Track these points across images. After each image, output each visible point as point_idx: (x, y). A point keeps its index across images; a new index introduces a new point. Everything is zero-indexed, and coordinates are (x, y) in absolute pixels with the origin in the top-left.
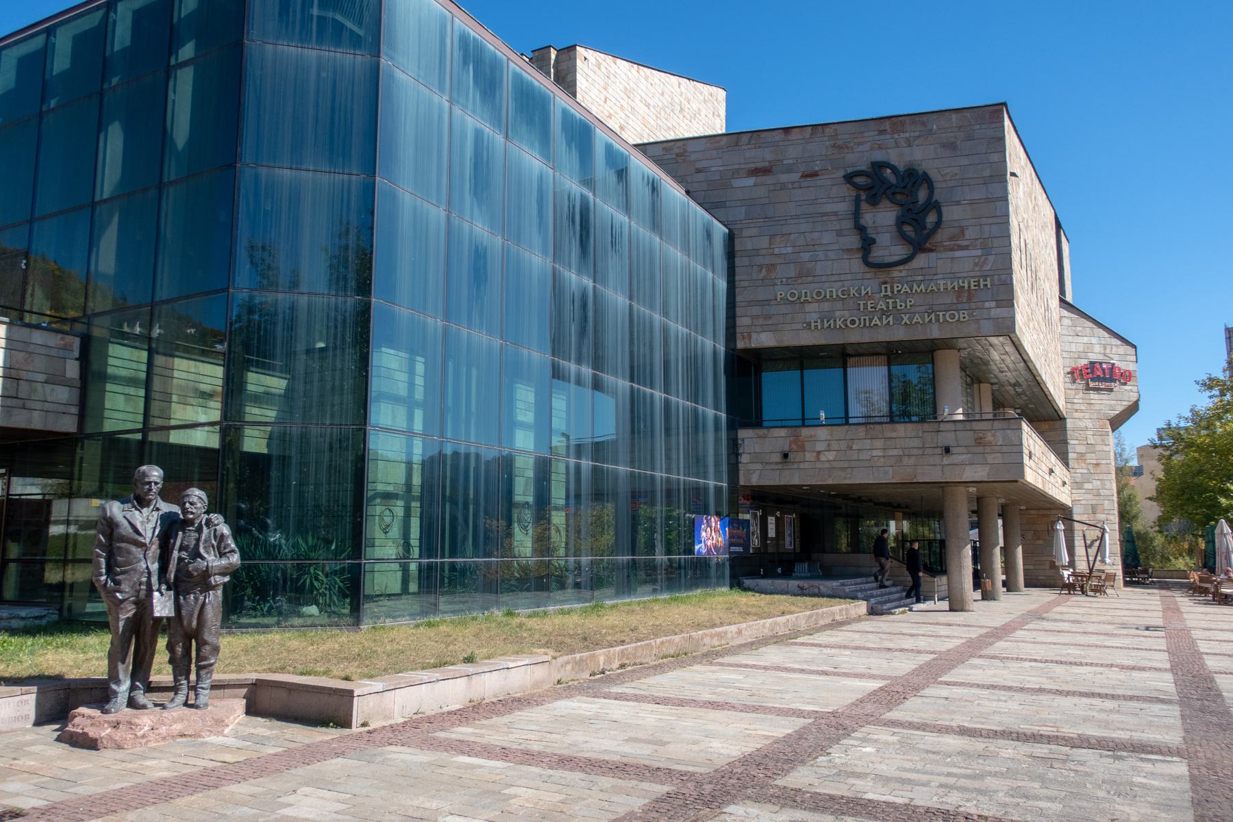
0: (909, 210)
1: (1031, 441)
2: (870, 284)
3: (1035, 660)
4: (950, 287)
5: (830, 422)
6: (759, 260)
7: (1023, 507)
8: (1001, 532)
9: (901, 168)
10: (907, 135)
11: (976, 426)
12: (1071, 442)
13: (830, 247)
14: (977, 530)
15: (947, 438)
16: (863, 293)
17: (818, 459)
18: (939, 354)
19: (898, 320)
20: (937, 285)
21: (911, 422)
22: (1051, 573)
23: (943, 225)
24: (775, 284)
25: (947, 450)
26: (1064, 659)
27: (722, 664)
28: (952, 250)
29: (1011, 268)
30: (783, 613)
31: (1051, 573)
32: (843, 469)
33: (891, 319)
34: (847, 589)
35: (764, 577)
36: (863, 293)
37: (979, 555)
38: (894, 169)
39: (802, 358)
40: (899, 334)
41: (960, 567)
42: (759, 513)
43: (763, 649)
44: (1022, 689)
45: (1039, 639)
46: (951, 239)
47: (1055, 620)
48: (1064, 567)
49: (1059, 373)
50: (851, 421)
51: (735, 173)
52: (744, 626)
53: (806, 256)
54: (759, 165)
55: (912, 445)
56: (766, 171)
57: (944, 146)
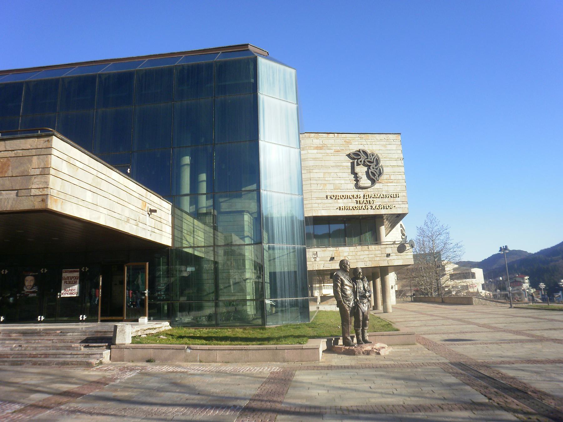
15: (389, 251)
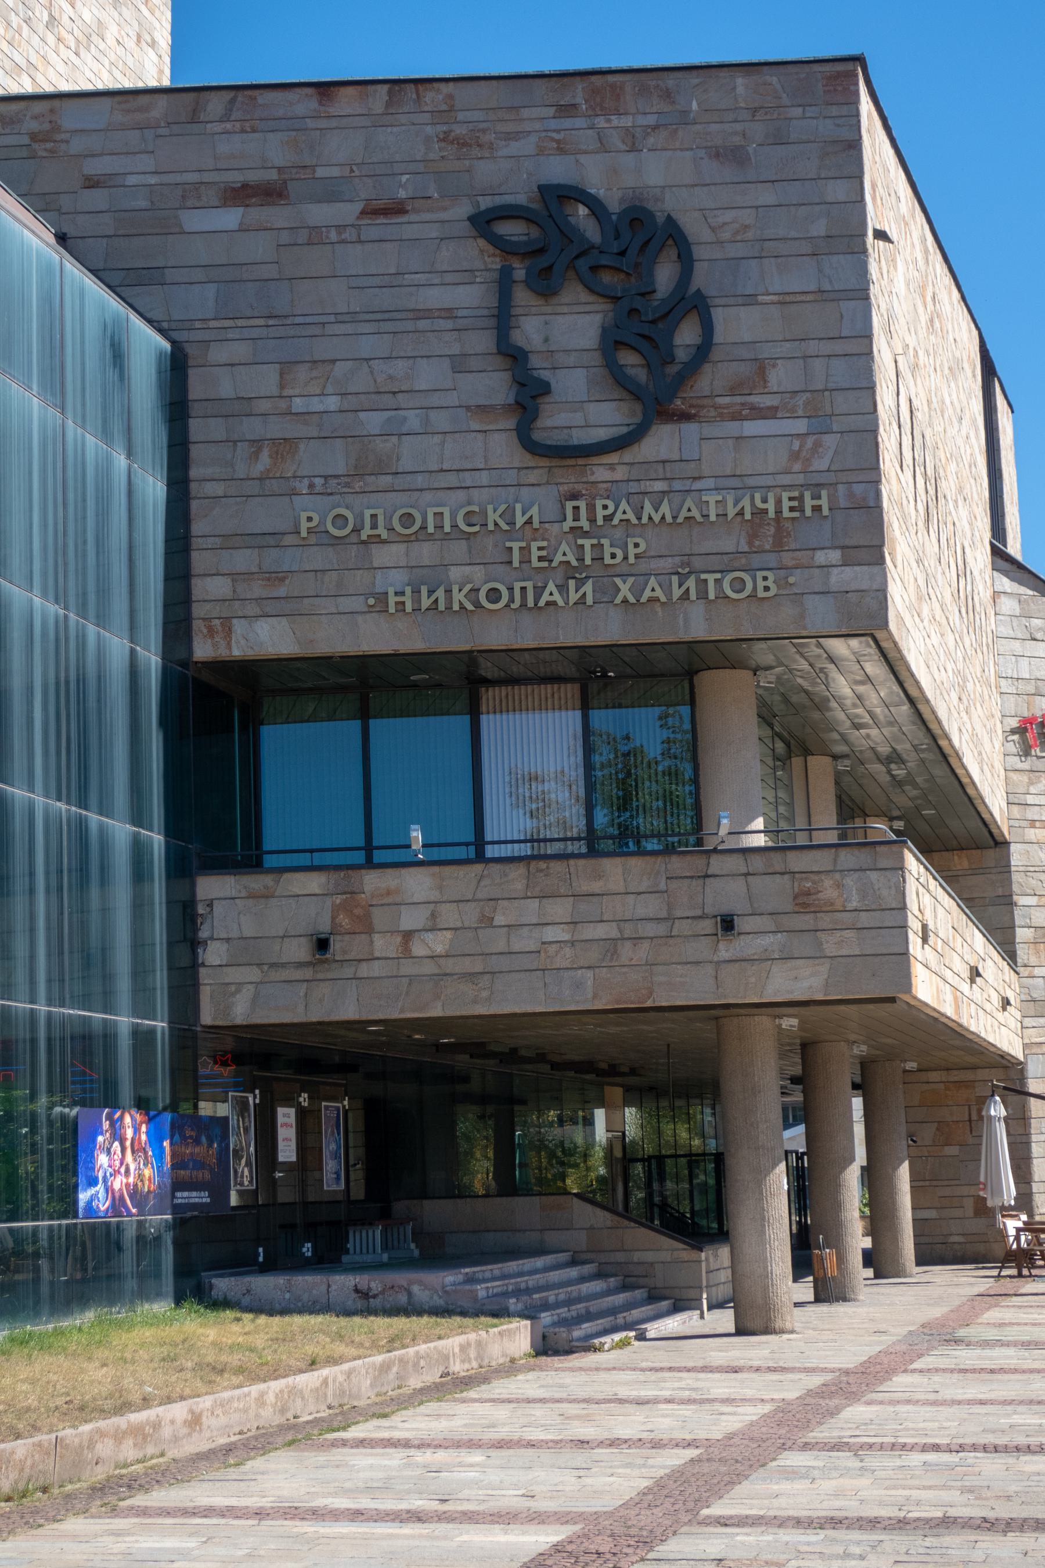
0: (633, 311)
1: (926, 899)
2: (537, 502)
3: (936, 1448)
4: (731, 512)
5: (436, 854)
6: (251, 428)
7: (911, 1065)
8: (859, 1130)
9: (614, 205)
10: (627, 121)
11: (799, 862)
12: (1022, 900)
13: (436, 400)
14: (801, 1129)
15: (727, 893)
16: (520, 521)
17: (406, 952)
18: (709, 681)
19: (607, 594)
20: (702, 505)
21: (642, 853)
22: (977, 1225)
23: (716, 354)
24: (294, 493)
25: (727, 924)
26: (1001, 1440)
27: (143, 1512)
28: (737, 417)
29: (875, 468)
30: (313, 1364)
31: (977, 1225)
32: (471, 977)
33: (588, 588)
34: (481, 1290)
35: (269, 1267)
36: (520, 521)
37: (809, 1189)
38: (595, 206)
39: (365, 688)
40: (609, 629)
41: (762, 1220)
42: (253, 1099)
43: (257, 1463)
44: (902, 1524)
45: (947, 1394)
46: (732, 392)
47: (986, 1344)
48: (1007, 1211)
49: (991, 732)
50: (491, 851)
51: (190, 195)
52: (205, 1403)
53: (373, 422)
54: (254, 177)
55: (641, 912)
56: (270, 193)
57: (716, 154)
